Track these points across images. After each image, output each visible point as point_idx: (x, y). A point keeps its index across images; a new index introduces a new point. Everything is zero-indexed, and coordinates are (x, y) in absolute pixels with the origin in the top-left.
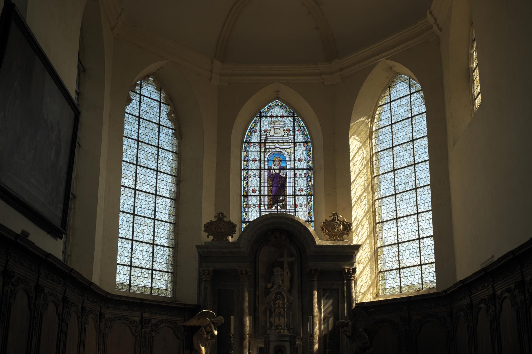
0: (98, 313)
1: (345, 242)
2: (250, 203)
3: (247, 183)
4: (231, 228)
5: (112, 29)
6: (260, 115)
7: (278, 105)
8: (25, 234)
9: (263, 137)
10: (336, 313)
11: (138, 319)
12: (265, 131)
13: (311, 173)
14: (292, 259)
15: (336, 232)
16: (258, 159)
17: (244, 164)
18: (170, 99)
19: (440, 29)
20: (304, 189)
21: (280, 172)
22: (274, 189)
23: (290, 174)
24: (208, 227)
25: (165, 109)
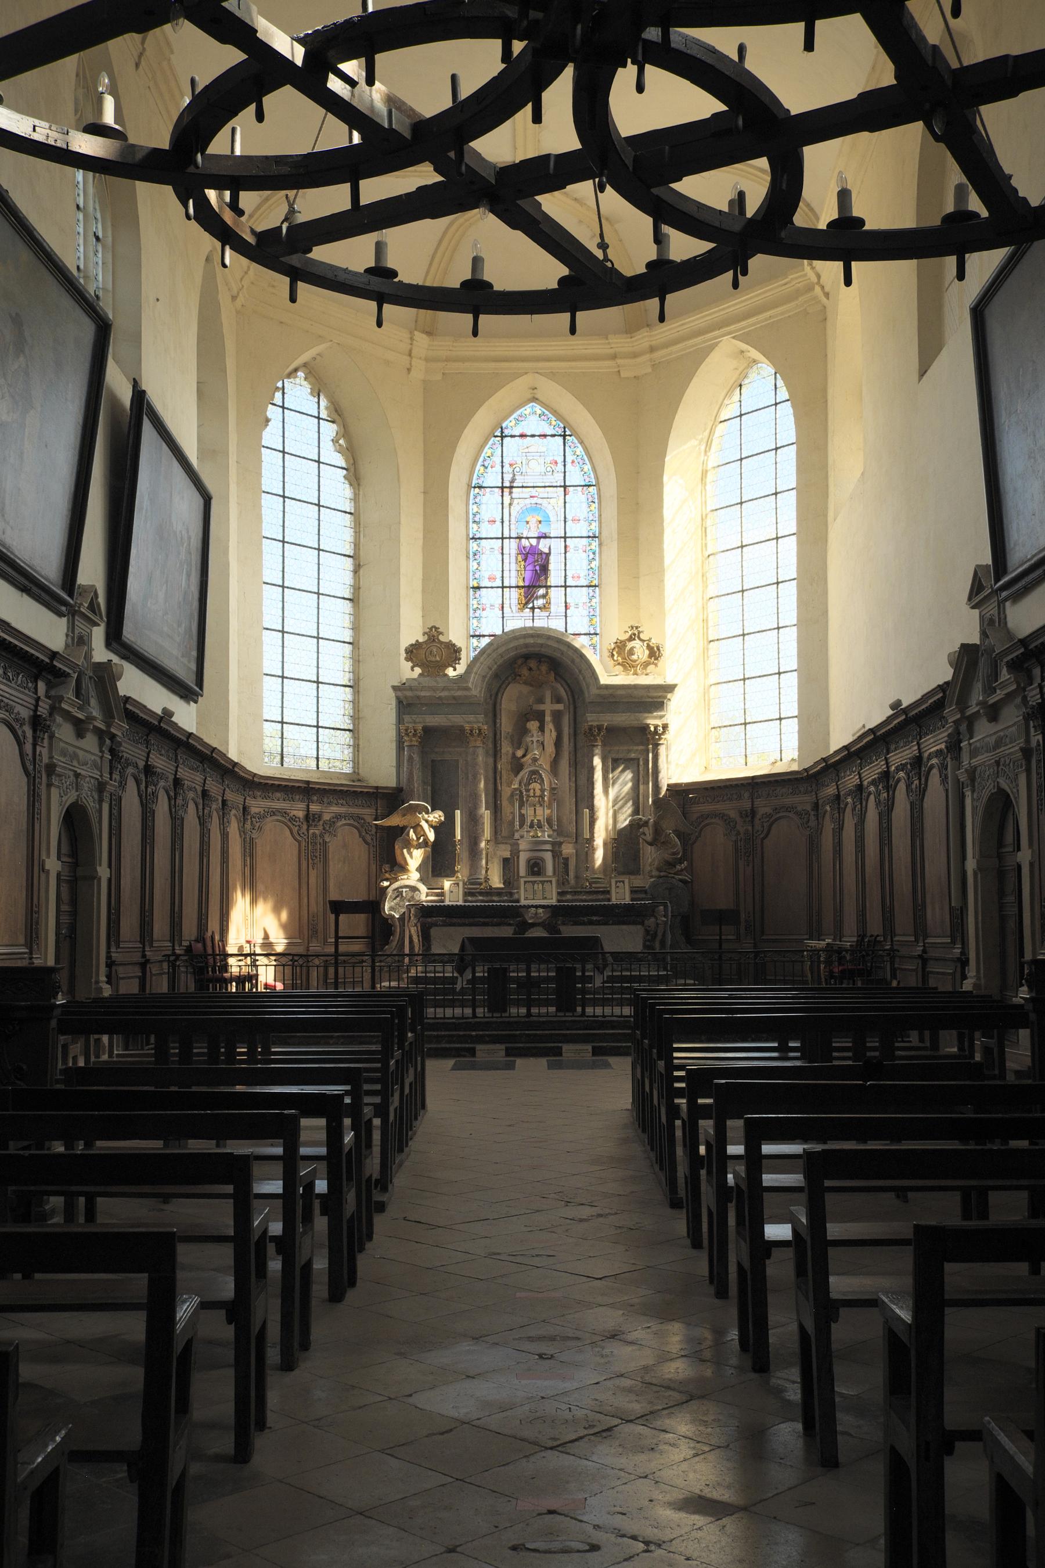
0: (241, 807)
2: (483, 601)
3: (479, 564)
4: (453, 653)
5: (234, 298)
6: (502, 432)
7: (535, 413)
8: (168, 714)
9: (508, 478)
10: (636, 796)
11: (301, 814)
12: (511, 465)
13: (595, 544)
14: (560, 707)
15: (635, 661)
16: (498, 518)
17: (474, 528)
18: (336, 411)
19: (827, 295)
20: (582, 575)
21: (538, 543)
22: (528, 575)
23: (557, 546)
24: (412, 652)
25: (329, 430)
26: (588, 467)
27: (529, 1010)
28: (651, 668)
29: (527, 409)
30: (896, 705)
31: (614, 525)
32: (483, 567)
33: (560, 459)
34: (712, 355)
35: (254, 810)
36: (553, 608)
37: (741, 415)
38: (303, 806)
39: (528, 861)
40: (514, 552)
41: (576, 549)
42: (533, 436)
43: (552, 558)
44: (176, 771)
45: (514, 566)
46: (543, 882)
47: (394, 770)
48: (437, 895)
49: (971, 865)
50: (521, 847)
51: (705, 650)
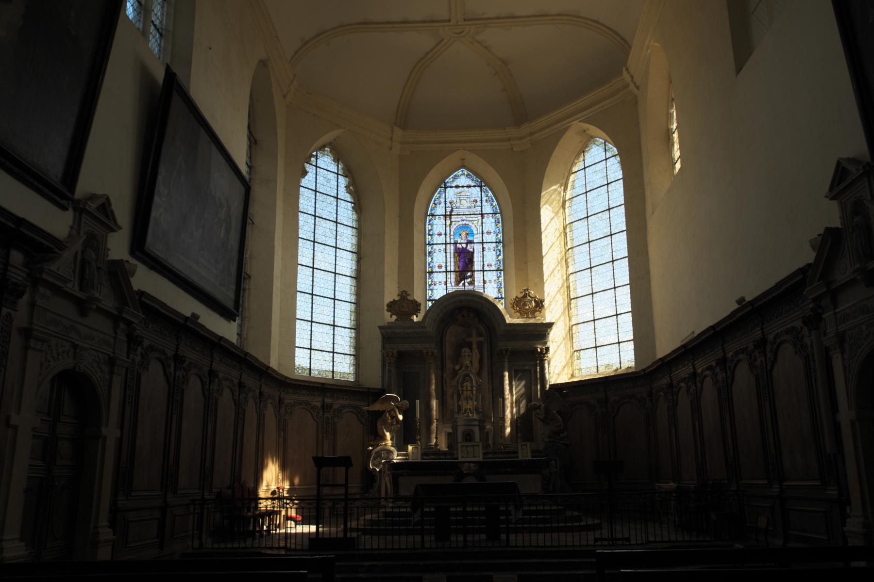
0: (277, 399)
1: (538, 320)
2: (435, 280)
4: (416, 307)
5: (284, 97)
8: (195, 317)
9: (449, 210)
10: (528, 395)
11: (319, 405)
13: (500, 246)
14: (481, 339)
16: (443, 232)
17: (428, 238)
19: (638, 88)
22: (461, 264)
23: (477, 248)
25: (343, 181)
26: (495, 203)
27: (465, 538)
28: (537, 313)
29: (459, 172)
30: (740, 301)
31: (512, 233)
32: (435, 259)
33: (479, 199)
34: (565, 136)
35: (287, 401)
36: (476, 284)
37: (585, 168)
38: (320, 399)
39: (464, 432)
40: (452, 252)
41: (489, 249)
42: (463, 187)
43: (475, 255)
44: (177, 348)
45: (452, 260)
46: (473, 446)
47: (380, 379)
48: (404, 455)
49: (846, 415)
50: (459, 424)
51: (569, 304)
